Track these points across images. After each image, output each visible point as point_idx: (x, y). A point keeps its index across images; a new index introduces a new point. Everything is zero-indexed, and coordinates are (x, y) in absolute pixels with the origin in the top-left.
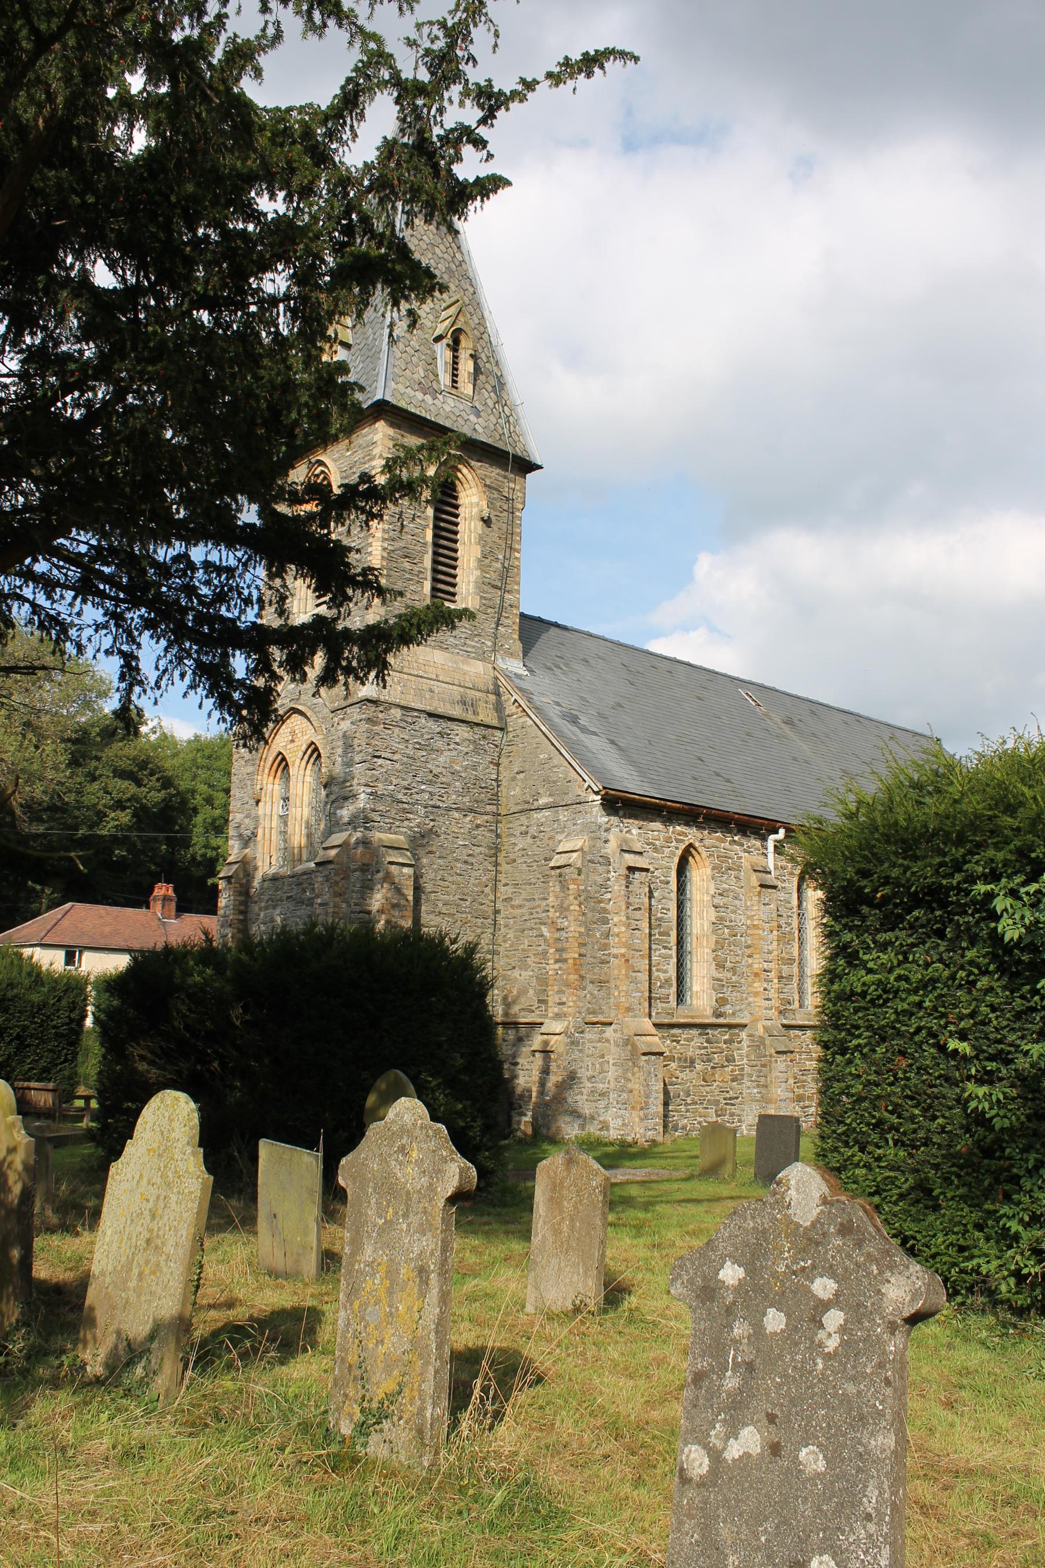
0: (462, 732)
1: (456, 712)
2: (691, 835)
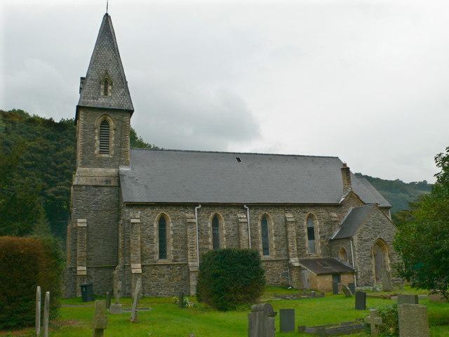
0: (106, 189)
1: (104, 184)
2: (163, 211)
